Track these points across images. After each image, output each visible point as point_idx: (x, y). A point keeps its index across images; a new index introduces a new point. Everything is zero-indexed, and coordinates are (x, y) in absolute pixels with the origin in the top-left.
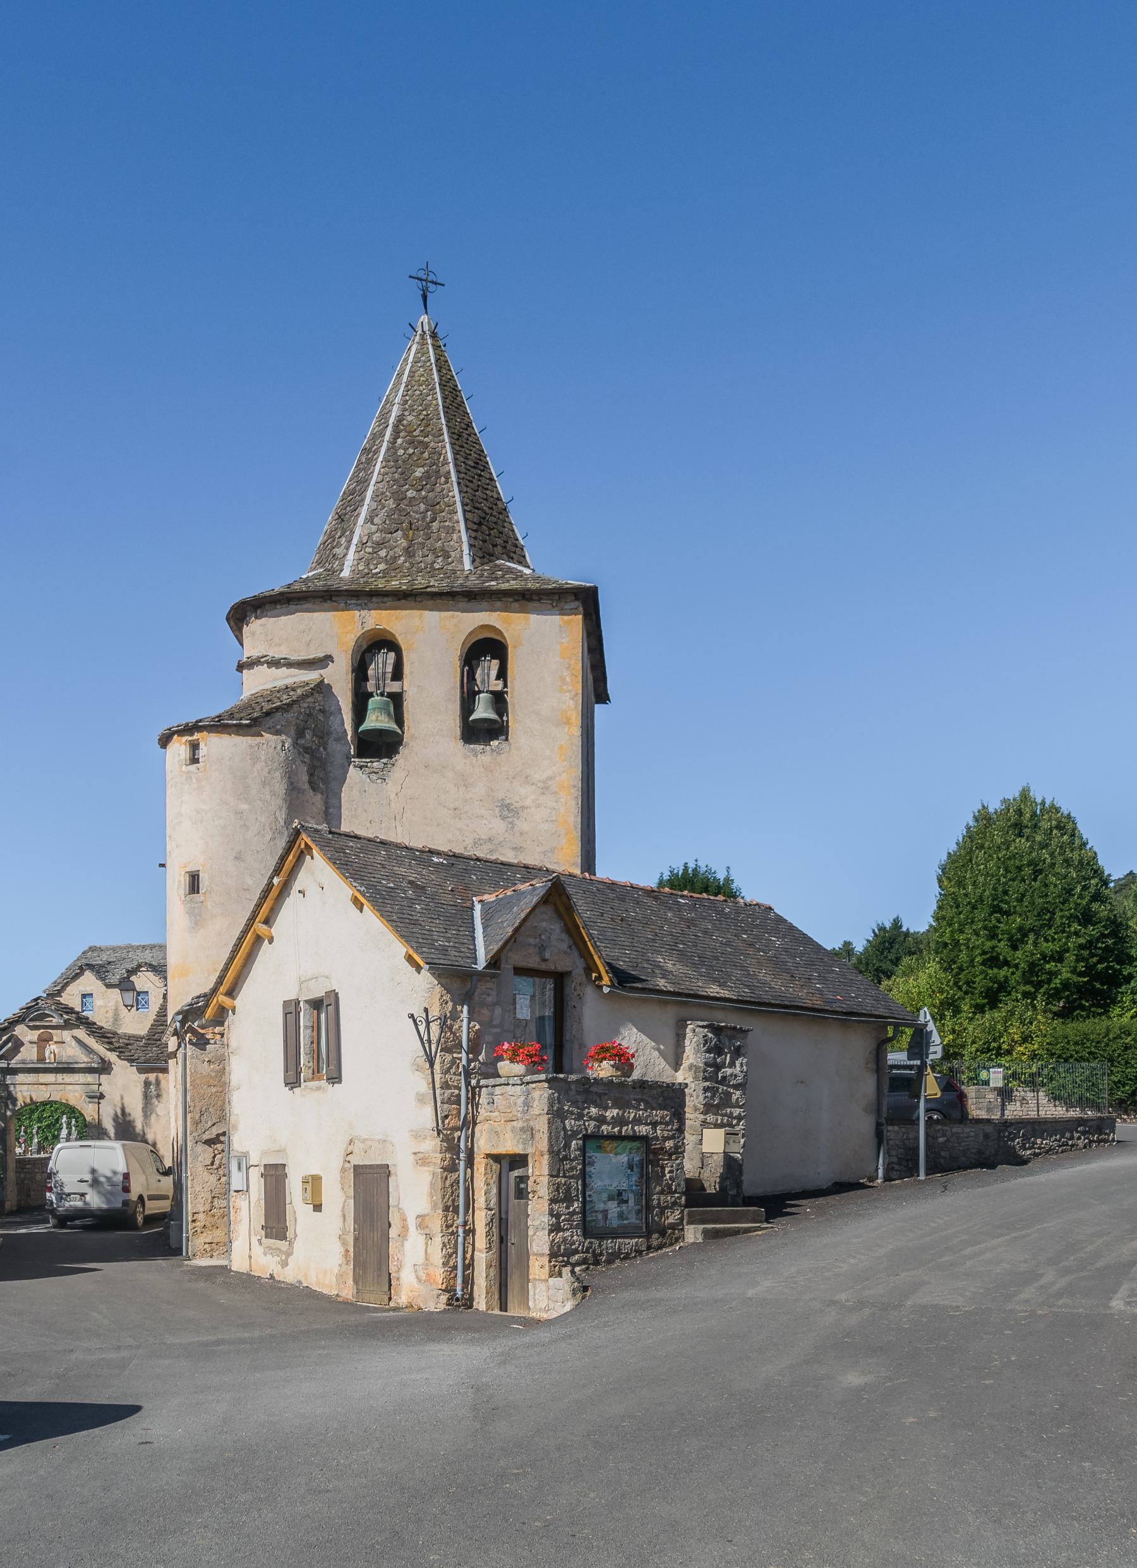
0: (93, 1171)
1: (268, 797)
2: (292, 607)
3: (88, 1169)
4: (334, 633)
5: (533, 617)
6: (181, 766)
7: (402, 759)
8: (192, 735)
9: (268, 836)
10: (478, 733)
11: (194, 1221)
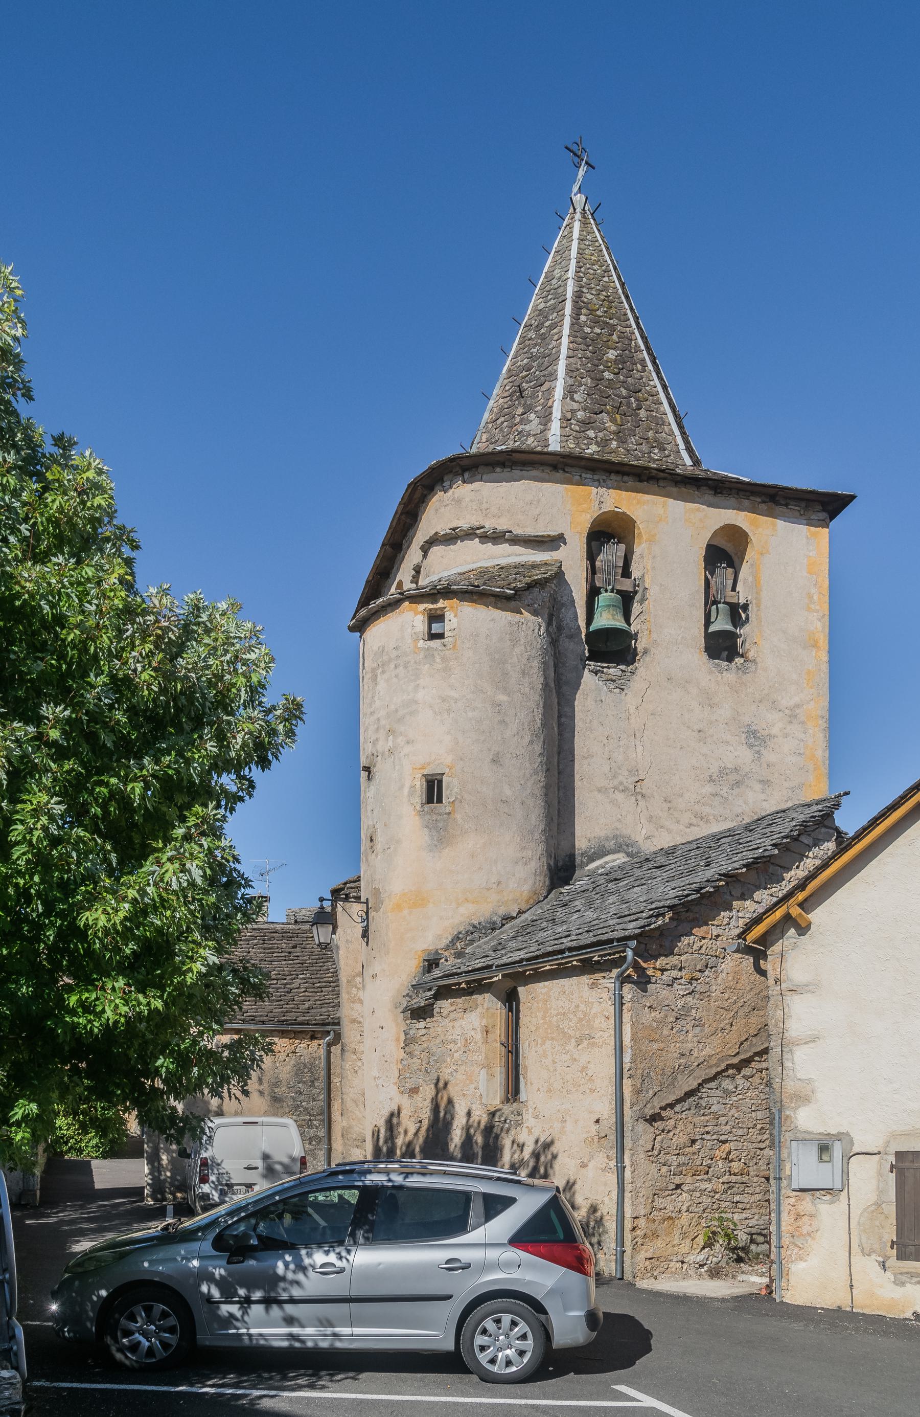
0: (266, 1157)
1: (527, 690)
2: (517, 473)
3: (259, 1154)
4: (566, 509)
5: (780, 523)
6: (416, 641)
7: (642, 667)
8: (435, 601)
9: (527, 739)
10: (723, 647)
11: (634, 1229)
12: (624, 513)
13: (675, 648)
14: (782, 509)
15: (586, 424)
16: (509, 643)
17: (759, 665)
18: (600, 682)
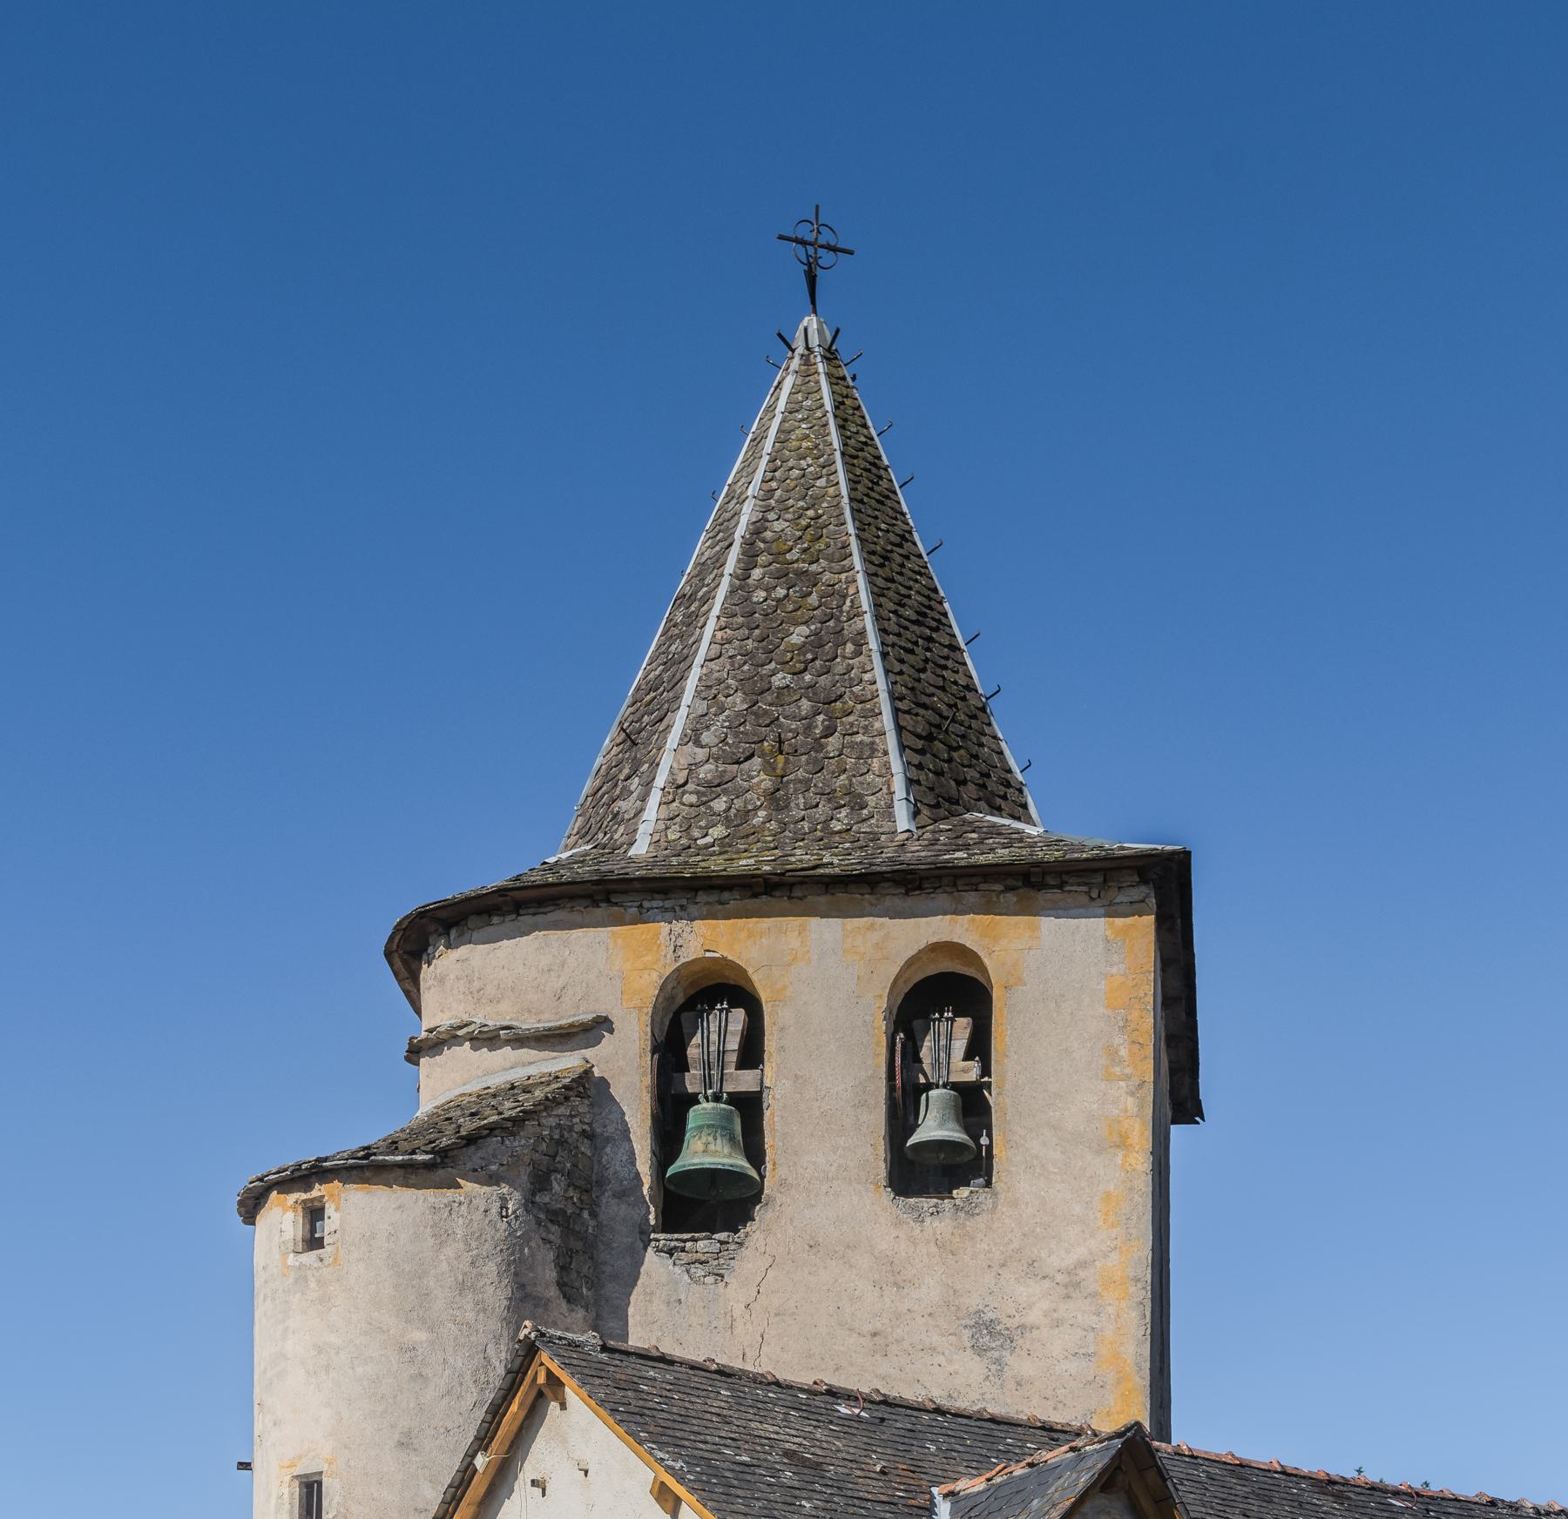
1: (470, 1316)
2: (527, 919)
4: (612, 972)
5: (1047, 924)
6: (285, 1255)
8: (308, 1188)
12: (724, 959)
13: (824, 1188)
14: (1055, 895)
15: (715, 786)
16: (431, 1241)
17: (1002, 1197)
18: (677, 1270)
